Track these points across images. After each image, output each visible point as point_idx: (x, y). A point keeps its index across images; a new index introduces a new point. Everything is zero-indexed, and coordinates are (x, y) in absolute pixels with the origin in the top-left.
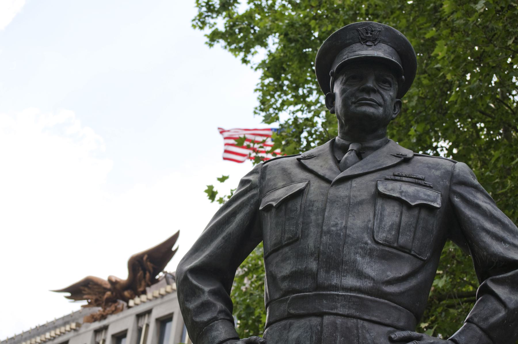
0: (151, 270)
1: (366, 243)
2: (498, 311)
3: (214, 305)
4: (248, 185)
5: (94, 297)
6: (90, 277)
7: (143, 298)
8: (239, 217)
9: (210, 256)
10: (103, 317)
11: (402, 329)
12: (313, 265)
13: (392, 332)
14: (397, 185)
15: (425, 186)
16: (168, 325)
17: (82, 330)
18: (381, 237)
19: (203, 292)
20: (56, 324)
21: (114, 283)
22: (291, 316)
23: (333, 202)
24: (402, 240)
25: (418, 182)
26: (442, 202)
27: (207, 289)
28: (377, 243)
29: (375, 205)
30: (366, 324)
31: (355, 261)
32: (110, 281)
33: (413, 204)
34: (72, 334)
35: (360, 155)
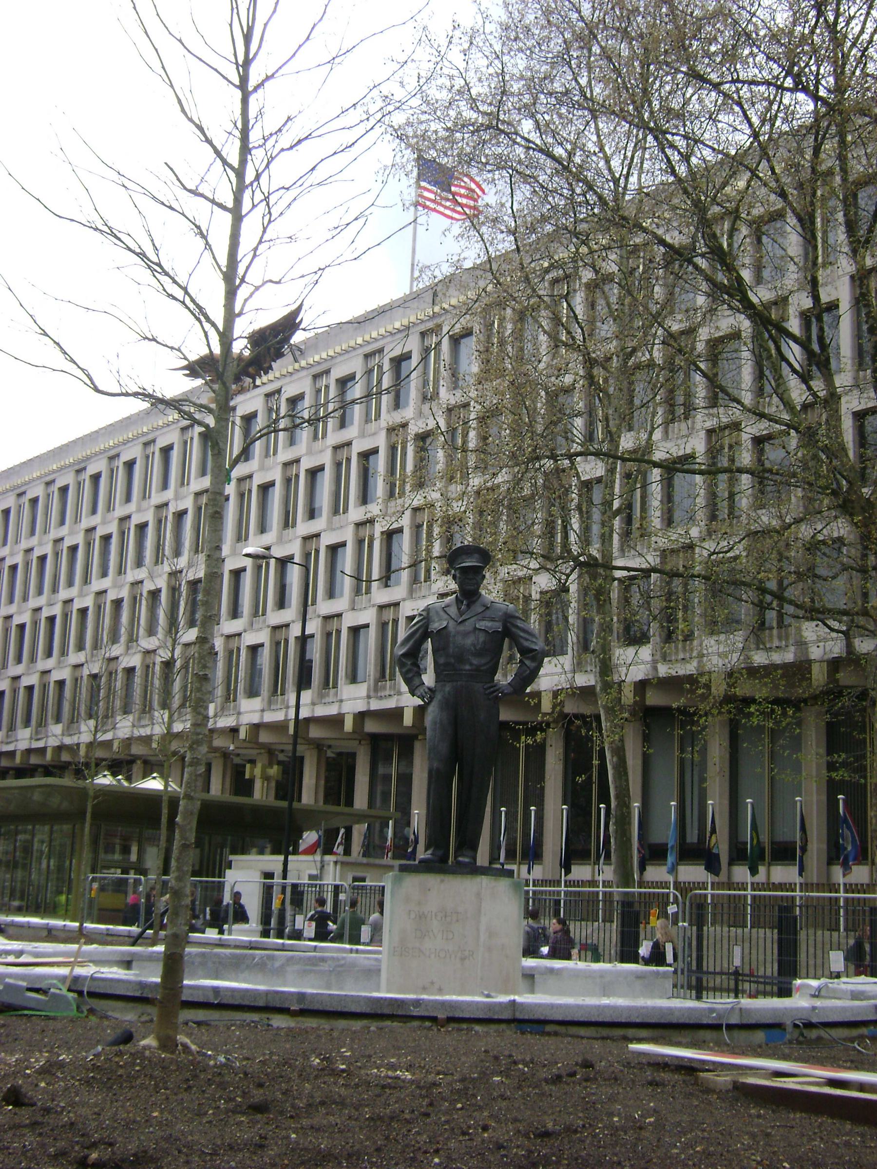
7: (271, 376)
8: (420, 631)
12: (452, 661)
25: (493, 620)
35: (468, 606)
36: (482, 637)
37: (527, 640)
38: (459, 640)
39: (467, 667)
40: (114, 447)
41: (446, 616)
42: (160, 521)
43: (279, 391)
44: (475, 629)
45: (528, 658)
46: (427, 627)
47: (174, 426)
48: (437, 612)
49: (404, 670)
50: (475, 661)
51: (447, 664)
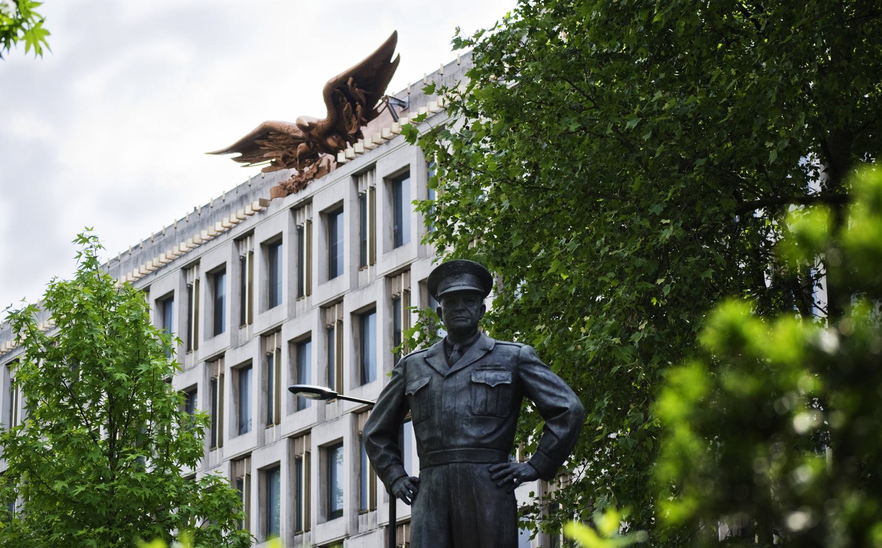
0: (362, 97)
1: (468, 416)
2: (553, 441)
3: (389, 456)
4: (397, 376)
5: (281, 154)
6: (266, 122)
7: (359, 146)
8: (395, 398)
9: (381, 425)
10: (301, 185)
11: (497, 463)
12: (439, 434)
13: (490, 467)
14: (483, 373)
15: (501, 370)
16: (404, 183)
17: (272, 210)
18: (476, 410)
19: (381, 449)
20: (227, 202)
21: (308, 128)
22: (430, 466)
23: (446, 392)
24: (489, 410)
25: (496, 368)
26: (513, 379)
27: (382, 447)
28: (474, 415)
29: (471, 390)
30: (474, 465)
31: (463, 428)
32: (301, 127)
33: (493, 386)
34: (257, 218)
35: (461, 352)
36: (481, 395)
37: (552, 395)
38: (448, 402)
39: (461, 441)
40: (141, 279)
41: (428, 370)
42: (213, 383)
43: (372, 168)
44: (471, 383)
45: (554, 423)
46: (404, 390)
47: (224, 238)
48: (417, 366)
49: (375, 458)
50: (473, 432)
51: (430, 440)
